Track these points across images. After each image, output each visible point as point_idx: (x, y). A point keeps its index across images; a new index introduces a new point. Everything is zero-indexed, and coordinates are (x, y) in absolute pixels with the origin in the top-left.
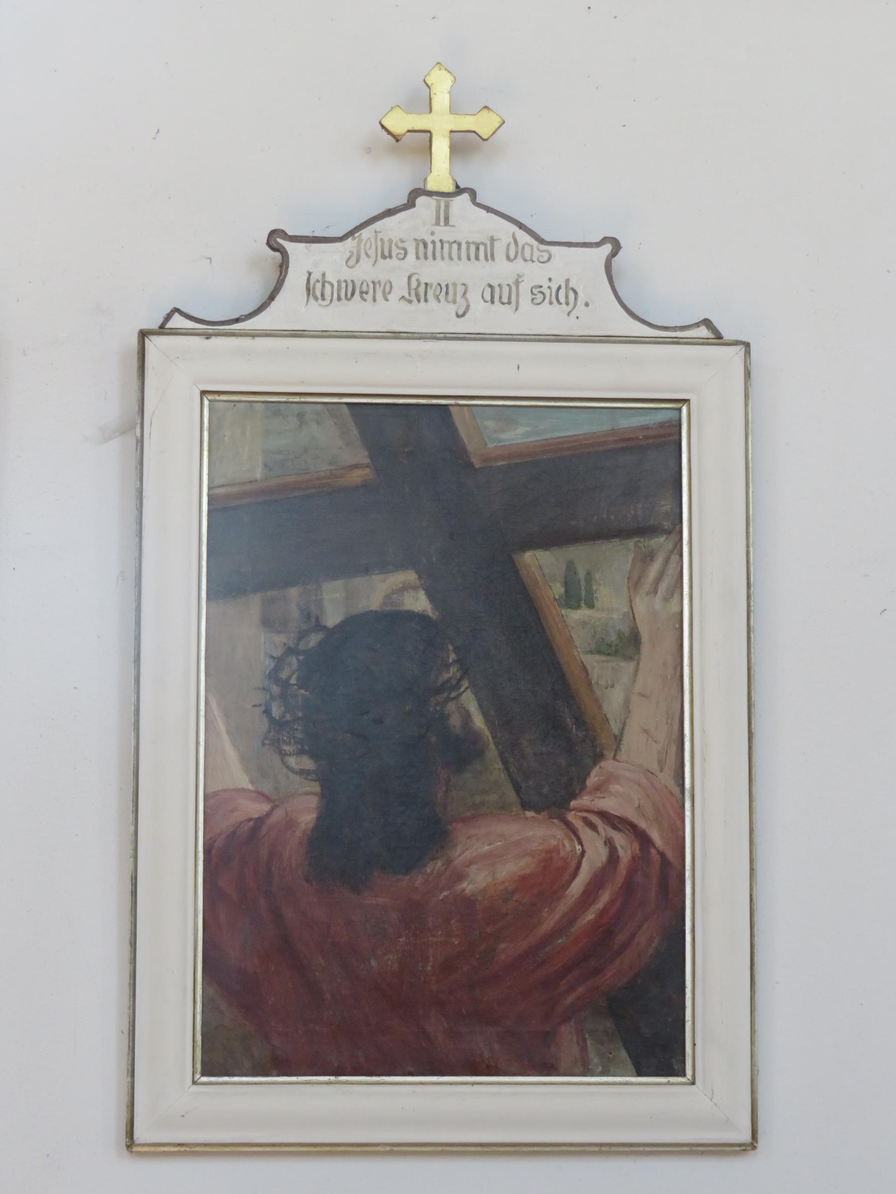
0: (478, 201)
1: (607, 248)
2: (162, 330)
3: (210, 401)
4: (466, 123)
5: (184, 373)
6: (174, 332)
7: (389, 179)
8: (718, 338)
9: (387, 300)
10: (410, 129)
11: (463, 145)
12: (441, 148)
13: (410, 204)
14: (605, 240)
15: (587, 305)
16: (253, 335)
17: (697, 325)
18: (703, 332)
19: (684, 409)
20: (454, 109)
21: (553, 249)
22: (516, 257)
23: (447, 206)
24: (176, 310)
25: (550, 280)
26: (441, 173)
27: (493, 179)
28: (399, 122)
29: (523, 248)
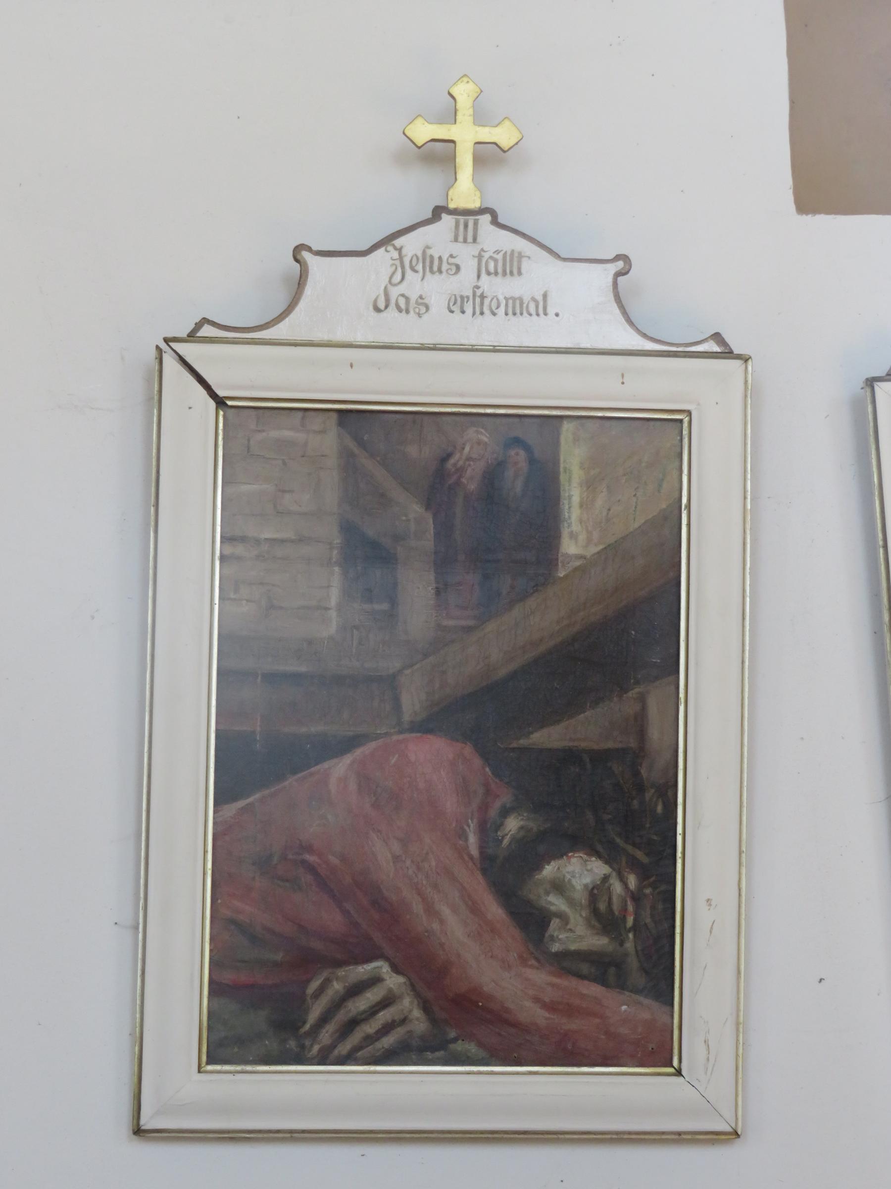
1: (306, 255)
2: (192, 337)
4: (486, 134)
7: (412, 192)
8: (728, 354)
11: (488, 157)
14: (618, 258)
21: (398, 242)
22: (386, 307)
23: (476, 223)
24: (205, 321)
27: (512, 194)
29: (487, 262)
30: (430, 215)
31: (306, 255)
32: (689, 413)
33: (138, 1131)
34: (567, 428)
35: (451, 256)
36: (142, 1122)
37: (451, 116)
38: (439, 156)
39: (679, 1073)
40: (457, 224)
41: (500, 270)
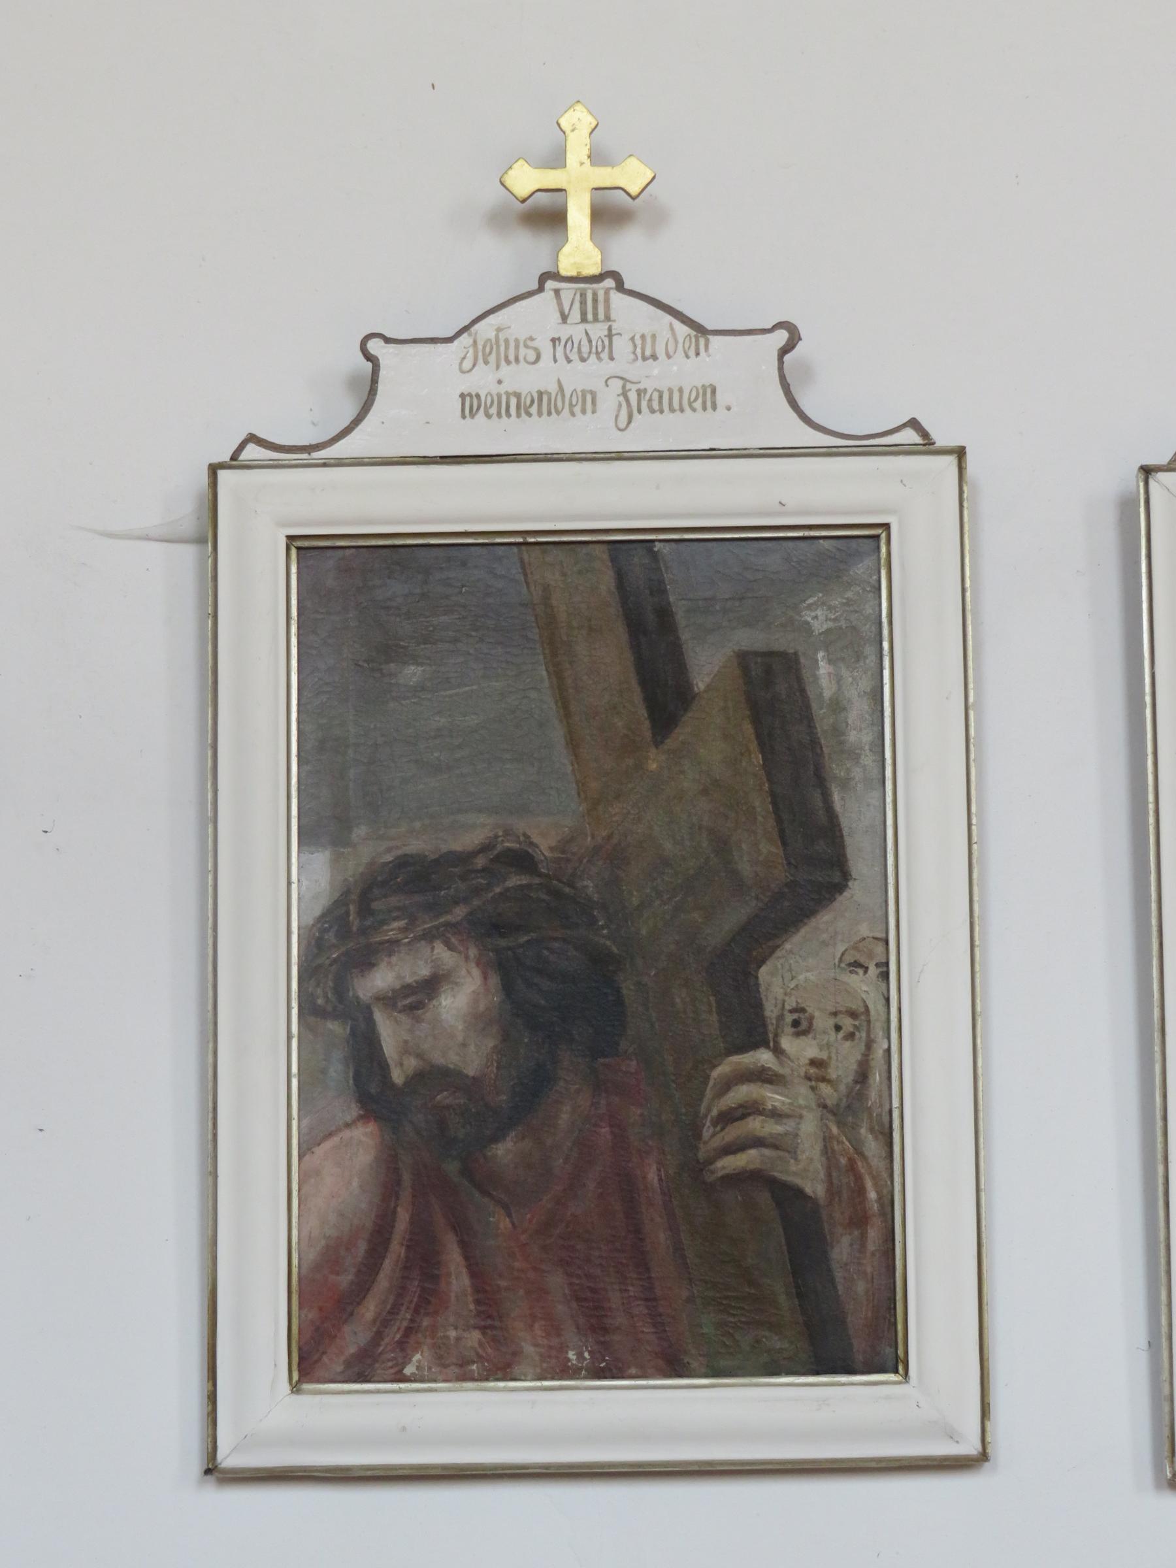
0: (626, 286)
2: (234, 462)
3: (298, 548)
4: (605, 176)
8: (927, 446)
11: (608, 214)
12: (578, 217)
13: (541, 289)
15: (729, 409)
16: (340, 463)
17: (904, 426)
18: (909, 436)
19: (883, 536)
20: (597, 157)
24: (252, 438)
26: (579, 250)
27: (632, 253)
28: (525, 180)
30: (536, 286)
31: (374, 346)
32: (886, 526)
33: (212, 1470)
34: (875, 557)
35: (532, 339)
36: (220, 1456)
37: (557, 159)
38: (547, 217)
40: (583, 295)
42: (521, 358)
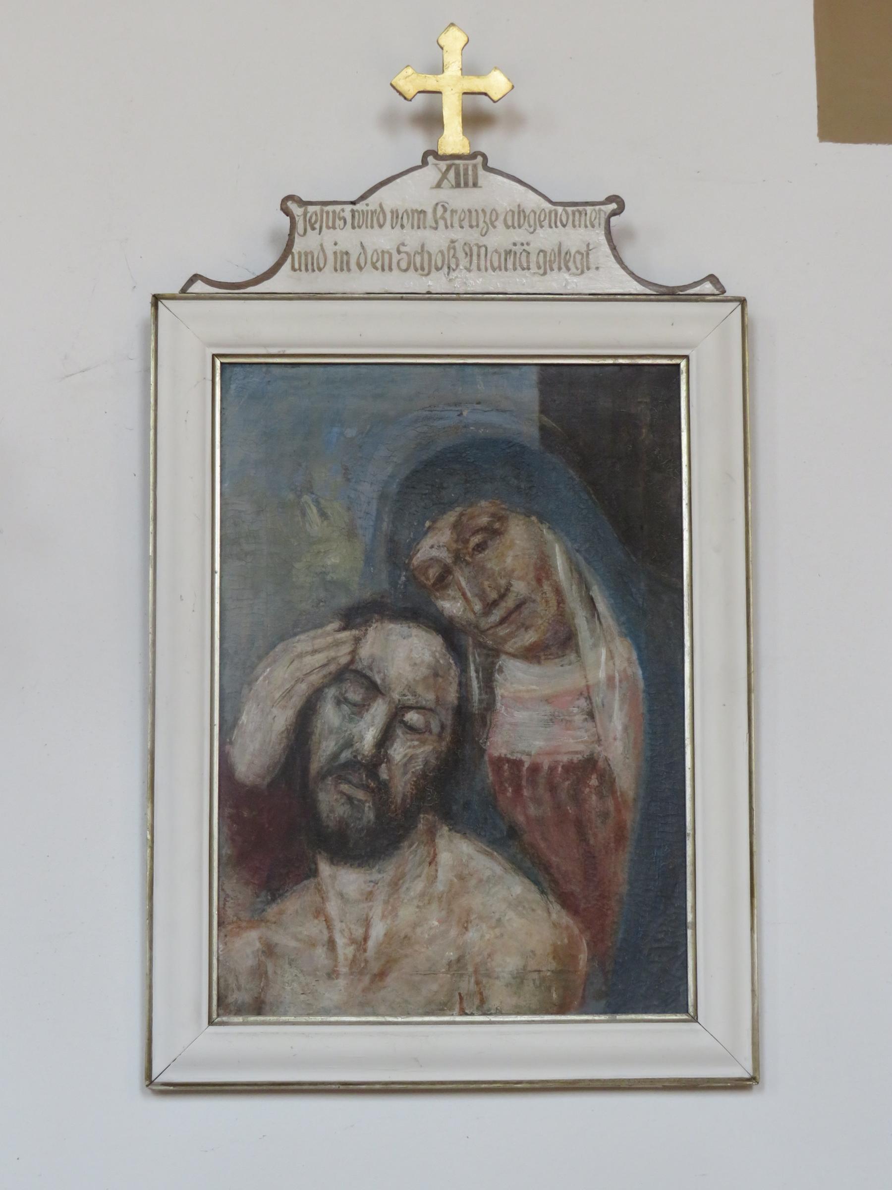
0: (490, 164)
2: (184, 294)
4: (475, 84)
5: (200, 334)
6: (199, 297)
8: (720, 295)
9: (494, 227)
10: (421, 89)
13: (425, 163)
14: (610, 199)
18: (708, 288)
20: (468, 70)
25: (336, 244)
26: (453, 139)
28: (410, 81)
32: (687, 357)
33: (153, 1084)
37: (439, 69)
39: (695, 1019)
41: (516, 225)
42: (337, 226)
